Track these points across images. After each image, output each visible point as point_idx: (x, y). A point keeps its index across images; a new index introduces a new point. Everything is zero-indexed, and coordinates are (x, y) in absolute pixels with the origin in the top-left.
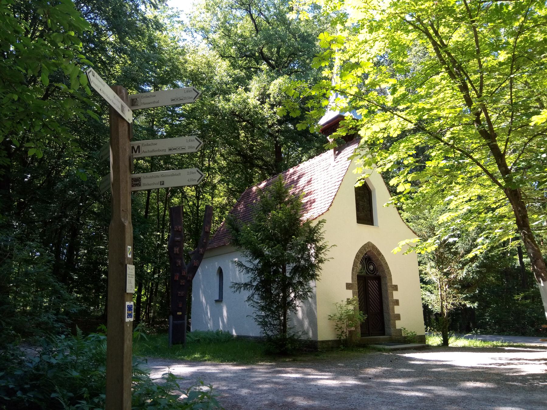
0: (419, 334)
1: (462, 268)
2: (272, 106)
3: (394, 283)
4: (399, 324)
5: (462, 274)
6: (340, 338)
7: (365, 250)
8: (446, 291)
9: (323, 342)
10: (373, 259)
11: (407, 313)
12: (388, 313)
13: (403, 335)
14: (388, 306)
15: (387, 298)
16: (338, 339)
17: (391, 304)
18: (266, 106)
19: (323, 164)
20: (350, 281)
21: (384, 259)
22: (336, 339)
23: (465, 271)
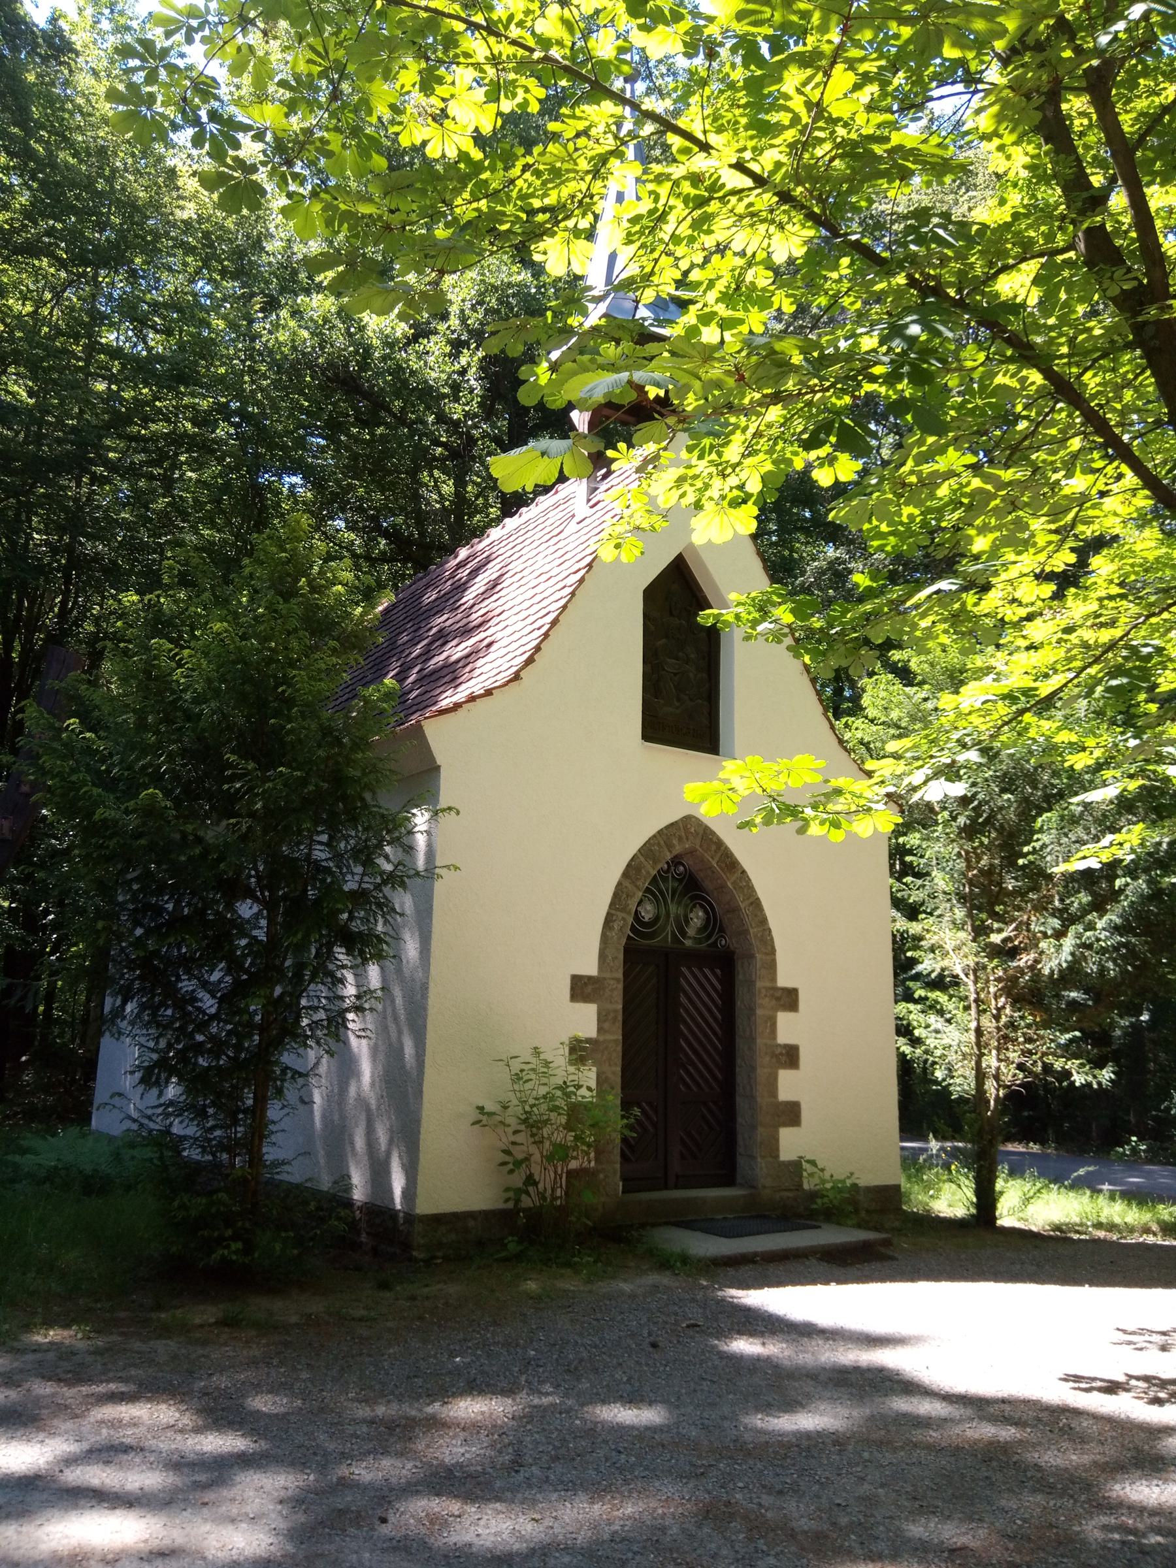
0: (867, 1179)
1: (1059, 934)
2: (457, 346)
3: (783, 981)
4: (791, 1143)
5: (1055, 956)
6: (517, 1201)
7: (670, 847)
8: (997, 1018)
9: (437, 1220)
10: (708, 885)
11: (829, 1094)
12: (752, 1098)
13: (806, 1186)
14: (753, 1068)
15: (752, 1039)
16: (510, 1205)
17: (763, 1062)
18: (436, 346)
19: (556, 516)
20: (590, 968)
21: (751, 888)
22: (501, 1205)
23: (1068, 943)
